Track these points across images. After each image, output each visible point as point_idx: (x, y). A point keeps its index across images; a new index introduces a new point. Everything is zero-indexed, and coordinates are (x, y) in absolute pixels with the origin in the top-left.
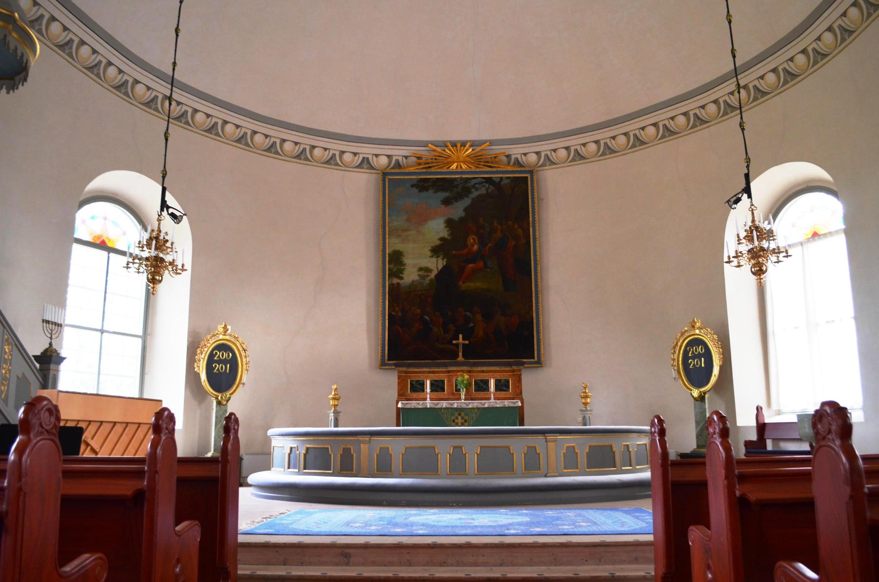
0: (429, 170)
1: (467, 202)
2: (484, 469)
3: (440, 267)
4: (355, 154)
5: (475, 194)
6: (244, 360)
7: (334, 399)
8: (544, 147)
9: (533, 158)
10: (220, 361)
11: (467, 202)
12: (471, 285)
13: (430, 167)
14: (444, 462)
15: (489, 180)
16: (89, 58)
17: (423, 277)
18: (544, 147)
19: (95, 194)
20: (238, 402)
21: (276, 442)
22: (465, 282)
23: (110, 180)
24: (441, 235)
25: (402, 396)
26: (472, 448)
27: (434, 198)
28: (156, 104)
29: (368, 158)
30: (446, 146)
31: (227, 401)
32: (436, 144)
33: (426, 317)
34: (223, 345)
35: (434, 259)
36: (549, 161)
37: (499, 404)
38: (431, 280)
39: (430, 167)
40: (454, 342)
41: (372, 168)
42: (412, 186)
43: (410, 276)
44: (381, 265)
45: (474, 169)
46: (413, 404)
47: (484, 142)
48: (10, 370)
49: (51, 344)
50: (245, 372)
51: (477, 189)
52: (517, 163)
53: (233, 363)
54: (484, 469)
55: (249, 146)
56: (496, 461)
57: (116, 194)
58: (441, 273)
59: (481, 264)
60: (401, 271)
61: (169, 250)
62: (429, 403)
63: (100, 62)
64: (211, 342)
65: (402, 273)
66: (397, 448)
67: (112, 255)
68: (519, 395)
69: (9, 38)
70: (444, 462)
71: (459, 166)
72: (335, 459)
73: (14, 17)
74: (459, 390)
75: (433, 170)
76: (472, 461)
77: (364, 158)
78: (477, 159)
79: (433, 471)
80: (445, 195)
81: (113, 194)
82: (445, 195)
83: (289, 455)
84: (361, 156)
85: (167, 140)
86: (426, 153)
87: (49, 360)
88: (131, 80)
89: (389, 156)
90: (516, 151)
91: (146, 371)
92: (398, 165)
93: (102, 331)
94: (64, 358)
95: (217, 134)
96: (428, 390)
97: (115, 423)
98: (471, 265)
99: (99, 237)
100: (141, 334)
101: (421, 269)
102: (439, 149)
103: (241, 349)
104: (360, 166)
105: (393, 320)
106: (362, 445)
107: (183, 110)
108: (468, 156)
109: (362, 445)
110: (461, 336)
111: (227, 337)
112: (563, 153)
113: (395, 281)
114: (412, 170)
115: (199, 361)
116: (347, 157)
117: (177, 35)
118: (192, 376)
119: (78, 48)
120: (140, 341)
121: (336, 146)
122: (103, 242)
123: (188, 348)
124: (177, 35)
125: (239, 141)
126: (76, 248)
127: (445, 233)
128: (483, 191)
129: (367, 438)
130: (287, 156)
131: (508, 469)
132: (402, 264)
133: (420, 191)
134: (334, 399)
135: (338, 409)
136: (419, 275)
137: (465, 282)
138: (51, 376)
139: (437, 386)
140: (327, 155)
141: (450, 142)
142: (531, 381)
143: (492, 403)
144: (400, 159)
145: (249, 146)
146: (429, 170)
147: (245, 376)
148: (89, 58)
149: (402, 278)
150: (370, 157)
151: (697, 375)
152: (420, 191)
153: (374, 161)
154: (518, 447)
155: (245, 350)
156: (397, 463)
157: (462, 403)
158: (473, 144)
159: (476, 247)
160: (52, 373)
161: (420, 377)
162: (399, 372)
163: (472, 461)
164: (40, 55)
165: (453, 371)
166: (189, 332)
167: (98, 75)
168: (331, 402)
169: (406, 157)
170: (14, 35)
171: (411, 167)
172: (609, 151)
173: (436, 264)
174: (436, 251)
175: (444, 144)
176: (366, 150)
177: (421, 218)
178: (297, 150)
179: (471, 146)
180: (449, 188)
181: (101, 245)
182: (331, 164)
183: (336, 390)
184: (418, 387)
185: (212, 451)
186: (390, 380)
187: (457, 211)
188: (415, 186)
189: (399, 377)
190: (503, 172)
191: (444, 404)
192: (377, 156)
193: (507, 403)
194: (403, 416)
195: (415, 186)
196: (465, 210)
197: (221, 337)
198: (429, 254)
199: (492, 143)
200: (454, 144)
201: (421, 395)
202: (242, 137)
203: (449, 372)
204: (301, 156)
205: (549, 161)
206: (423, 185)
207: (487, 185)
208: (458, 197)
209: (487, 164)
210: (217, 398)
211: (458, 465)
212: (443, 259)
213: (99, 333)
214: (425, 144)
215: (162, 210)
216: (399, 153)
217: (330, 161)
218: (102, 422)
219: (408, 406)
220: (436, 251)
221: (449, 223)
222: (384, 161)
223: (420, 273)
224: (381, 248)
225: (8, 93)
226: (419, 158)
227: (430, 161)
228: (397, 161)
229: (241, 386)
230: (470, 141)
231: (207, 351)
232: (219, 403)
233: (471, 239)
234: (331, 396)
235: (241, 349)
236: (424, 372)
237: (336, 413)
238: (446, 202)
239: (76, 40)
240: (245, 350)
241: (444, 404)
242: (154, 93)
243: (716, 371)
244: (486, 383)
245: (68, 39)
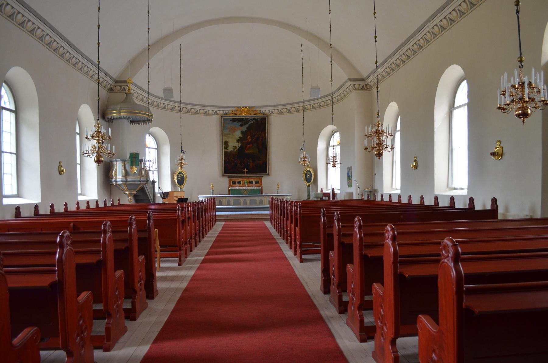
1: (247, 126)
2: (250, 204)
5: (250, 123)
8: (271, 109)
9: (268, 112)
11: (247, 126)
12: (248, 151)
14: (242, 202)
15: (254, 119)
17: (234, 149)
18: (271, 109)
20: (185, 186)
22: (247, 148)
25: (230, 186)
26: (248, 200)
27: (237, 124)
32: (237, 107)
36: (272, 113)
37: (256, 188)
43: (230, 149)
46: (233, 188)
52: (263, 113)
53: (183, 177)
54: (250, 204)
56: (252, 202)
58: (240, 148)
59: (251, 145)
60: (228, 147)
62: (237, 188)
68: (261, 185)
70: (242, 202)
71: (244, 115)
74: (245, 183)
76: (248, 202)
79: (239, 204)
80: (241, 123)
82: (241, 123)
90: (263, 109)
92: (226, 114)
105: (225, 162)
112: (276, 111)
116: (210, 112)
127: (241, 136)
128: (252, 122)
131: (256, 204)
132: (228, 145)
137: (247, 148)
139: (239, 183)
140: (204, 112)
142: (265, 180)
143: (254, 188)
147: (186, 181)
151: (308, 180)
153: (218, 112)
154: (258, 199)
156: (232, 203)
157: (246, 188)
161: (234, 180)
163: (248, 202)
172: (290, 112)
173: (238, 145)
174: (238, 141)
176: (216, 109)
177: (233, 130)
178: (195, 111)
180: (242, 121)
184: (234, 183)
186: (225, 181)
187: (244, 128)
188: (232, 120)
190: (260, 116)
191: (241, 188)
193: (258, 188)
194: (230, 192)
195: (232, 120)
196: (247, 128)
200: (243, 107)
204: (196, 113)
205: (272, 113)
206: (234, 120)
208: (245, 124)
209: (254, 114)
211: (245, 203)
216: (226, 110)
217: (205, 113)
220: (238, 141)
221: (242, 132)
222: (221, 112)
231: (176, 176)
232: (181, 188)
233: (249, 137)
238: (241, 126)
241: (241, 188)
243: (312, 179)
244: (253, 182)
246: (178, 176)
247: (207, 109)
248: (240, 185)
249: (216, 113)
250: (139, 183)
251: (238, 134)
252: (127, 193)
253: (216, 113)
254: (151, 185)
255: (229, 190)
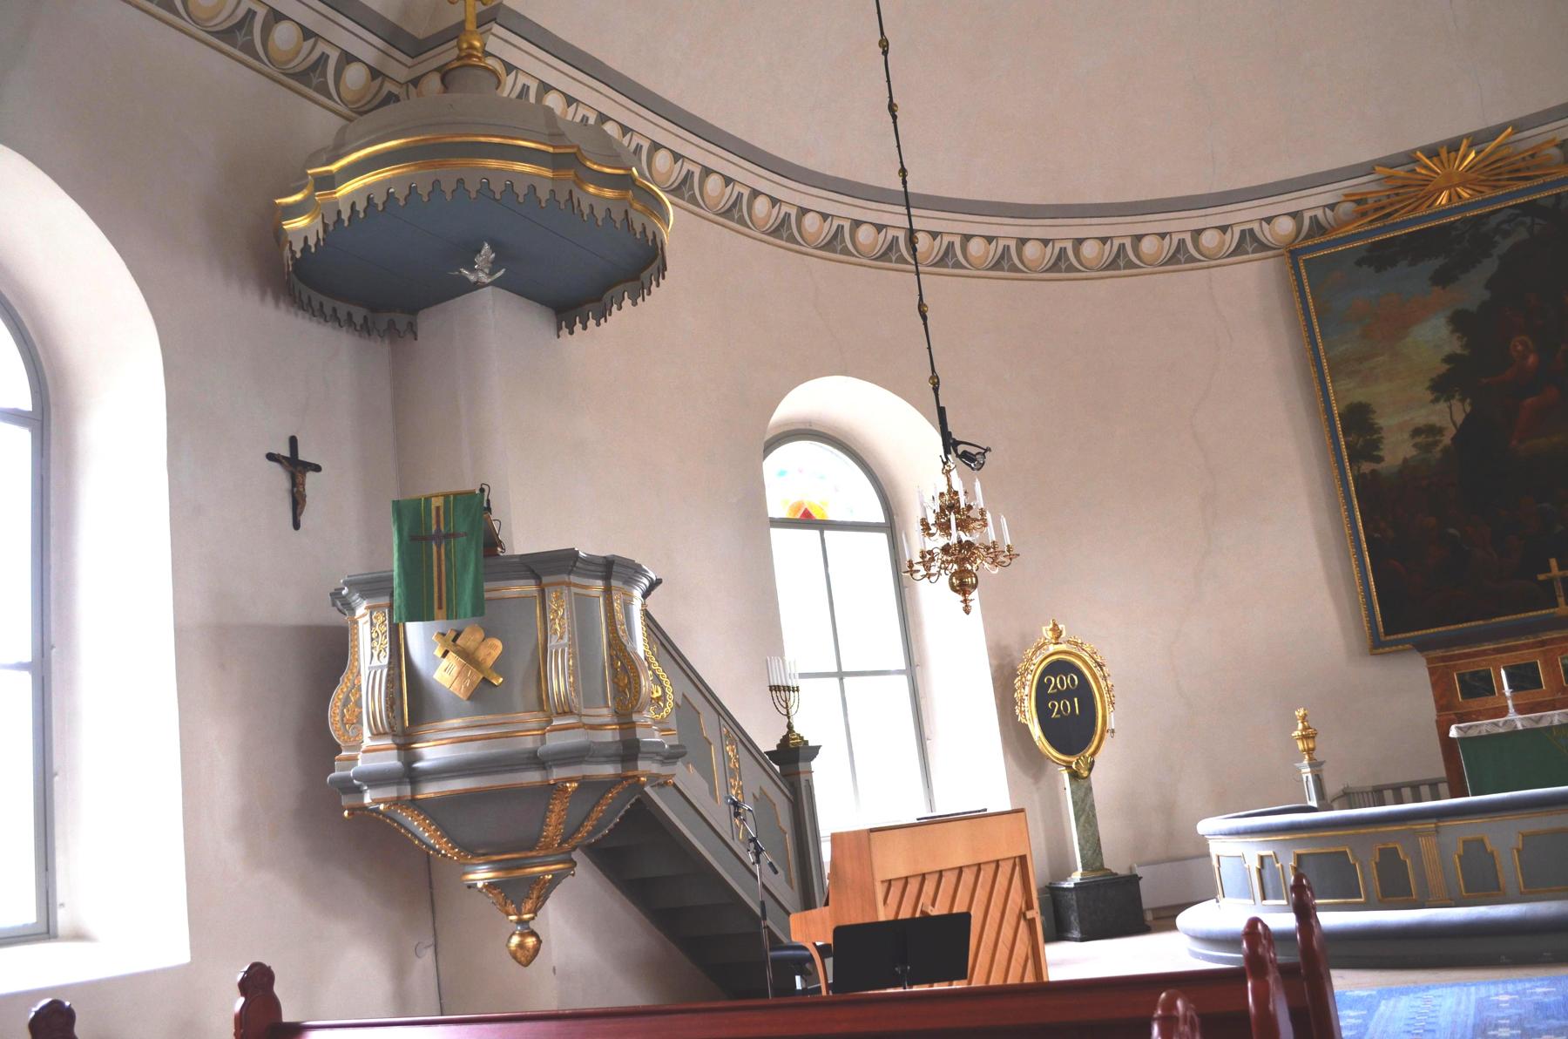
0: (1389, 221)
1: (1489, 266)
3: (1460, 418)
4: (1223, 229)
5: (1504, 245)
6: (1103, 684)
7: (1304, 737)
10: (1059, 695)
11: (1489, 266)
13: (1390, 214)
15: (1530, 208)
16: (821, 228)
17: (1426, 448)
19: (786, 429)
20: (1109, 765)
21: (1216, 847)
23: (811, 399)
24: (1447, 350)
25: (1447, 712)
28: (843, 240)
29: (1251, 230)
30: (1417, 161)
31: (1090, 770)
32: (1389, 162)
33: (1452, 531)
34: (1058, 662)
35: (1442, 405)
38: (1446, 450)
39: (1390, 214)
40: (1541, 577)
41: (1263, 247)
42: (1359, 263)
43: (1397, 450)
44: (1328, 441)
45: (1489, 193)
46: (1485, 726)
47: (1501, 128)
48: (741, 788)
49: (790, 726)
50: (1109, 708)
51: (1506, 234)
53: (1084, 692)
55: (1018, 270)
57: (810, 423)
60: (1376, 444)
61: (976, 524)
62: (1517, 720)
63: (740, 195)
64: (1036, 661)
65: (1378, 448)
66: (1504, 839)
67: (827, 533)
69: (632, 215)
72: (1366, 874)
73: (631, 176)
75: (1397, 218)
77: (1243, 232)
78: (1494, 171)
80: (1435, 263)
81: (803, 422)
82: (1435, 263)
83: (1260, 871)
84: (1237, 230)
85: (924, 318)
86: (1374, 187)
87: (793, 756)
88: (793, 212)
89: (1296, 215)
91: (927, 732)
92: (1317, 227)
93: (841, 675)
94: (818, 747)
95: (958, 265)
96: (1507, 691)
97: (961, 869)
98: (1529, 401)
99: (799, 506)
100: (903, 666)
101: (1417, 432)
102: (1400, 172)
103: (1093, 665)
104: (1239, 250)
106: (1422, 841)
107: (889, 238)
108: (1471, 168)
109: (1422, 841)
110: (1553, 562)
111: (1063, 647)
113: (1366, 467)
114: (1351, 229)
115: (1022, 700)
117: (895, 117)
118: (1013, 732)
119: (267, 30)
120: (904, 679)
121: (1180, 224)
122: (807, 514)
123: (994, 680)
124: (895, 117)
125: (997, 266)
126: (776, 534)
127: (1454, 345)
128: (1522, 234)
129: (1430, 825)
130: (1091, 269)
132: (1372, 429)
133: (1378, 270)
134: (1304, 737)
135: (1318, 756)
136: (1415, 445)
138: (803, 784)
139: (1523, 678)
141: (1423, 149)
144: (1319, 213)
145: (1018, 270)
146: (1389, 221)
147: (1110, 716)
148: (821, 228)
149: (1380, 459)
150: (1256, 226)
152: (1378, 270)
153: (1266, 233)
155: (1100, 666)
156: (1509, 868)
158: (1476, 139)
159: (1532, 359)
160: (803, 777)
161: (1478, 664)
162: (1429, 661)
164: (677, 228)
165: (1552, 641)
166: (989, 649)
167: (741, 221)
168: (1300, 746)
169: (1332, 207)
170: (637, 206)
171: (1347, 223)
173: (1448, 416)
174: (1442, 388)
175: (1410, 158)
176: (1244, 215)
178: (1109, 251)
179: (1471, 146)
181: (806, 520)
182: (1179, 262)
183: (1304, 718)
184: (1480, 685)
185: (1080, 870)
186: (1407, 686)
187: (1472, 290)
189: (1432, 672)
192: (1269, 220)
194: (1464, 765)
197: (1052, 648)
198: (1430, 396)
199: (1518, 125)
200: (1432, 152)
201: (1489, 702)
202: (1002, 257)
203: (1543, 643)
206: (1381, 256)
207: (1528, 220)
209: (1517, 174)
210: (1069, 767)
212: (1462, 401)
213: (836, 680)
214: (1368, 168)
215: (947, 452)
216: (1313, 202)
217: (1179, 257)
218: (941, 872)
219: (1473, 733)
220: (1442, 388)
221: (1459, 321)
222: (1285, 226)
223: (1419, 440)
224: (1321, 406)
225: (635, 304)
226: (1358, 202)
227: (1385, 201)
228: (1314, 219)
229: (1107, 735)
230: (1467, 136)
231: (1032, 679)
232: (1074, 776)
234: (1297, 733)
235: (1093, 665)
236: (1484, 653)
237: (1315, 765)
238: (1442, 278)
239: (697, 171)
240: (1100, 666)
242: (836, 223)
245: (684, 172)
246: (1042, 687)
247: (1180, 224)
248: (1531, 696)
249: (1249, 242)
250: (533, 777)
251: (1433, 339)
252: (481, 875)
253: (1249, 242)
254: (756, 782)
255: (1448, 745)
